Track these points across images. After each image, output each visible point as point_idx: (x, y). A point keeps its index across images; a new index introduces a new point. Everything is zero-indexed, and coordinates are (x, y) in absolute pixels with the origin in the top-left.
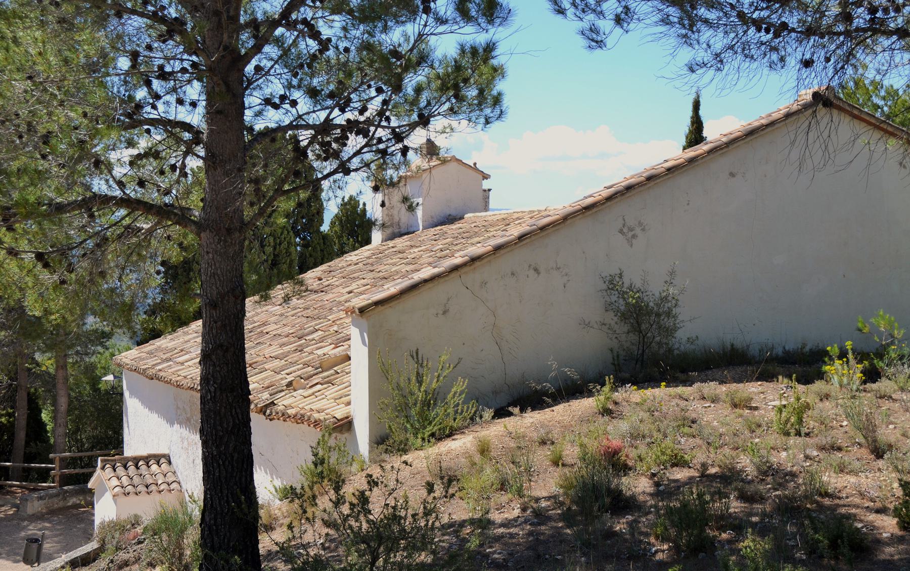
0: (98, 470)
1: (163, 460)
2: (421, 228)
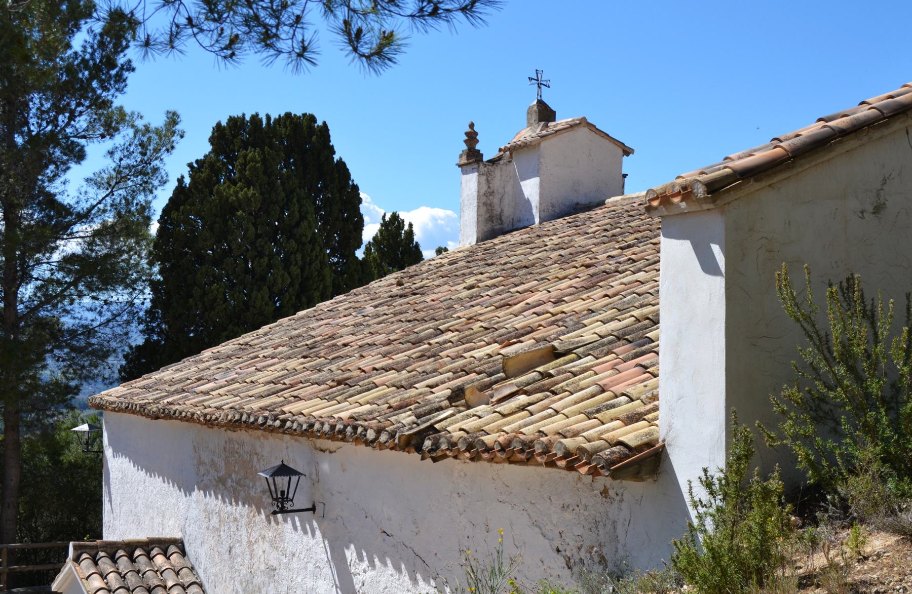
0: (70, 564)
1: (172, 549)
2: (537, 220)
